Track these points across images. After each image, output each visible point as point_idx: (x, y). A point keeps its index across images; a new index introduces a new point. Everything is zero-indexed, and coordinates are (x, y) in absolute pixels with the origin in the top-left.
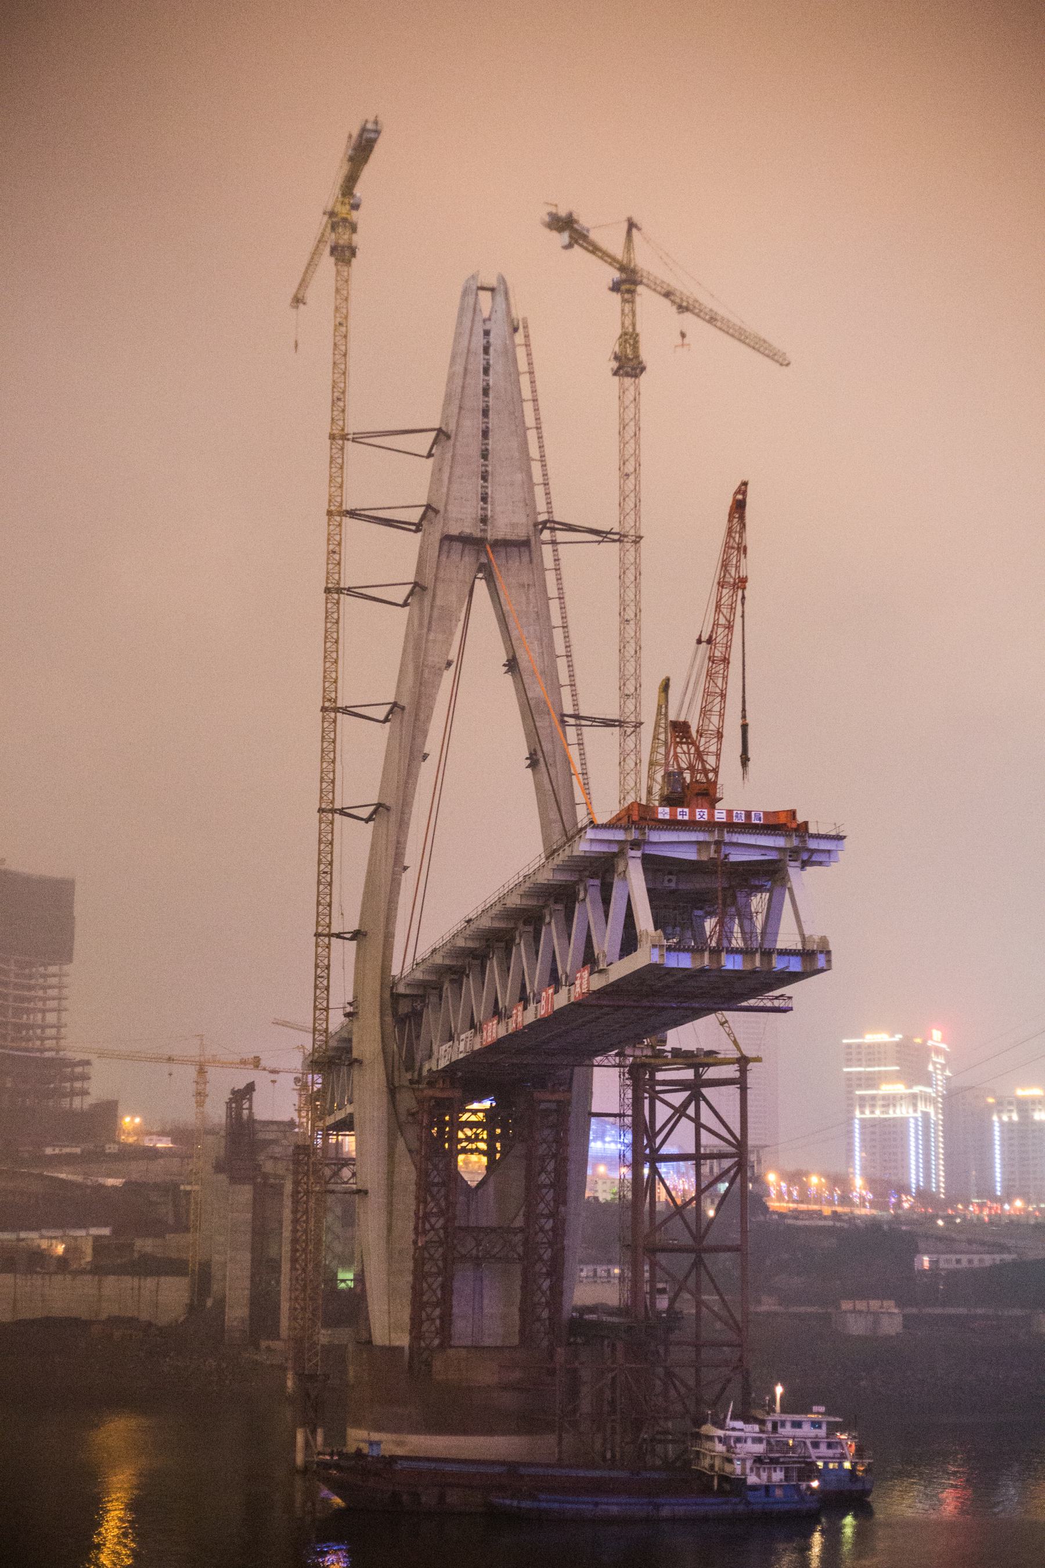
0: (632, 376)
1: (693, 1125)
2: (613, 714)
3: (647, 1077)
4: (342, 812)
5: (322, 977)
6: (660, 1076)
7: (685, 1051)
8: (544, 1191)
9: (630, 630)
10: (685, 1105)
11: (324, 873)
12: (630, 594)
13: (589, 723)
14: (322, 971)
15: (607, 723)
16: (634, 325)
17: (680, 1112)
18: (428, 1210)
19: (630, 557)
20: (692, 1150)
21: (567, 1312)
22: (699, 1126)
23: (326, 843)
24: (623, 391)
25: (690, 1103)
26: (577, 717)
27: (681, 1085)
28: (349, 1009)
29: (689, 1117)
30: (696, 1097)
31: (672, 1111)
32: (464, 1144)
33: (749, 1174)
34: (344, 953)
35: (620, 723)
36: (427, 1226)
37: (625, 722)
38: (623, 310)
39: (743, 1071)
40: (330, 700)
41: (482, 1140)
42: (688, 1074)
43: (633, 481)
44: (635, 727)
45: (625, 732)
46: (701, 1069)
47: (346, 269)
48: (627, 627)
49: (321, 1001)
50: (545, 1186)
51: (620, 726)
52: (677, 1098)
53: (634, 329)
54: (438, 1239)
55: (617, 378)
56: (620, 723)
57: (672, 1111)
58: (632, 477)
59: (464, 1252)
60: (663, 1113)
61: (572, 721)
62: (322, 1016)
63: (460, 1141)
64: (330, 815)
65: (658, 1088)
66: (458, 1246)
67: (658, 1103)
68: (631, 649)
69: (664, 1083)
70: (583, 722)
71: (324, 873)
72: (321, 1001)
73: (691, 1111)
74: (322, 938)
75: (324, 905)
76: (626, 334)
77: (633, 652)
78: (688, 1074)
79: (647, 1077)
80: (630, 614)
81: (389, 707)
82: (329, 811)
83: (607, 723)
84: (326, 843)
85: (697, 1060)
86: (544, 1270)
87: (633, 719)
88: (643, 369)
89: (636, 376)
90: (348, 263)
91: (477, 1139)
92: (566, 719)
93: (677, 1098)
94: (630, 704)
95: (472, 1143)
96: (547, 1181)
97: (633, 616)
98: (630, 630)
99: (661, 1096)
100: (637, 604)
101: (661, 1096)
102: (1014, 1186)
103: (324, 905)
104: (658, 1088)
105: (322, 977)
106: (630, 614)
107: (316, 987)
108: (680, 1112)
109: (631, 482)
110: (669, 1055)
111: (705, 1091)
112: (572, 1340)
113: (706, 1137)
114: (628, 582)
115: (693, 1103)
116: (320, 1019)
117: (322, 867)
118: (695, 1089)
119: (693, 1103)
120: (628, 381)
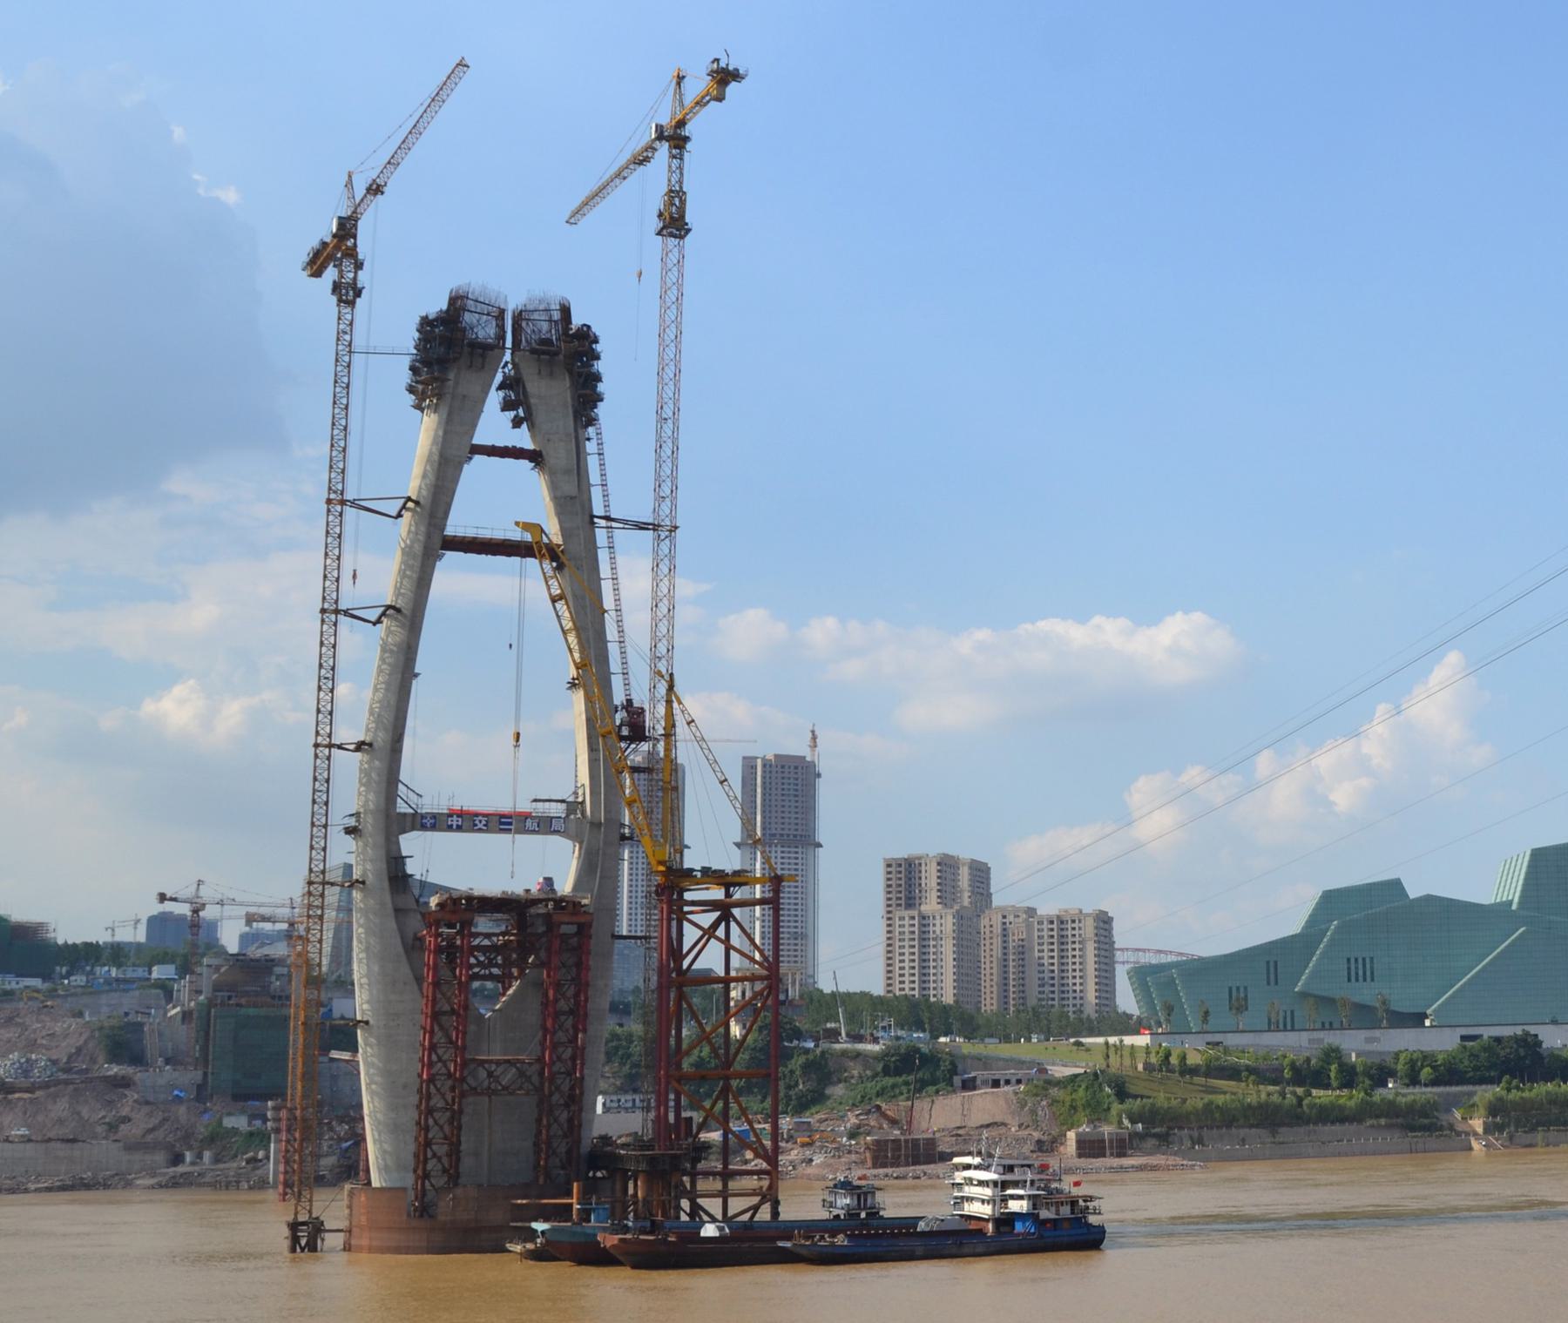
0: (675, 236)
1: (723, 946)
2: (647, 517)
3: (675, 897)
4: (346, 613)
5: (320, 791)
6: (688, 896)
7: (715, 871)
8: (563, 1018)
9: (668, 429)
10: (715, 925)
11: (326, 678)
12: (669, 392)
13: (621, 526)
14: (322, 785)
15: (641, 526)
16: (680, 182)
17: (709, 933)
18: (435, 1041)
19: (665, 547)
20: (720, 1200)
21: (586, 1146)
22: (728, 948)
23: (329, 646)
24: (666, 253)
25: (719, 924)
26: (608, 518)
27: (712, 905)
28: (352, 822)
29: (718, 939)
30: (726, 917)
31: (701, 933)
32: (476, 970)
33: (782, 997)
34: (348, 767)
35: (655, 527)
36: (434, 1057)
37: (659, 526)
38: (670, 167)
39: (777, 891)
40: (335, 492)
41: (496, 965)
42: (717, 894)
43: (671, 426)
44: (671, 531)
45: (659, 536)
46: (732, 889)
47: (349, 310)
48: (665, 426)
49: (316, 863)
50: (564, 1013)
51: (654, 530)
52: (707, 919)
53: (681, 187)
54: (445, 1072)
55: (660, 237)
56: (655, 527)
57: (701, 933)
58: (668, 501)
59: (474, 1084)
60: (690, 935)
61: (603, 523)
62: (320, 834)
63: (471, 967)
64: (327, 750)
65: (686, 909)
66: (469, 1078)
67: (685, 923)
68: (670, 372)
69: (693, 903)
70: (614, 524)
71: (326, 678)
72: (316, 863)
73: (721, 932)
74: (321, 749)
75: (326, 713)
76: (671, 191)
77: (667, 570)
78: (717, 894)
79: (675, 897)
80: (666, 490)
81: (403, 501)
82: (332, 611)
83: (641, 526)
84: (329, 646)
85: (730, 879)
86: (562, 1101)
87: (669, 523)
88: (689, 231)
89: (682, 237)
90: (352, 304)
91: (491, 964)
92: (596, 520)
93: (707, 919)
94: (666, 508)
95: (486, 969)
96: (566, 1008)
97: (671, 414)
98: (668, 429)
99: (689, 916)
100: (676, 402)
101: (689, 916)
102: (1053, 1006)
103: (326, 713)
104: (686, 909)
105: (320, 791)
106: (668, 412)
107: (314, 802)
108: (709, 933)
109: (669, 425)
110: (699, 875)
111: (736, 912)
112: (591, 1174)
113: (736, 959)
114: (664, 457)
115: (723, 923)
116: (319, 814)
117: (323, 672)
118: (724, 911)
119: (723, 923)
120: (672, 241)
